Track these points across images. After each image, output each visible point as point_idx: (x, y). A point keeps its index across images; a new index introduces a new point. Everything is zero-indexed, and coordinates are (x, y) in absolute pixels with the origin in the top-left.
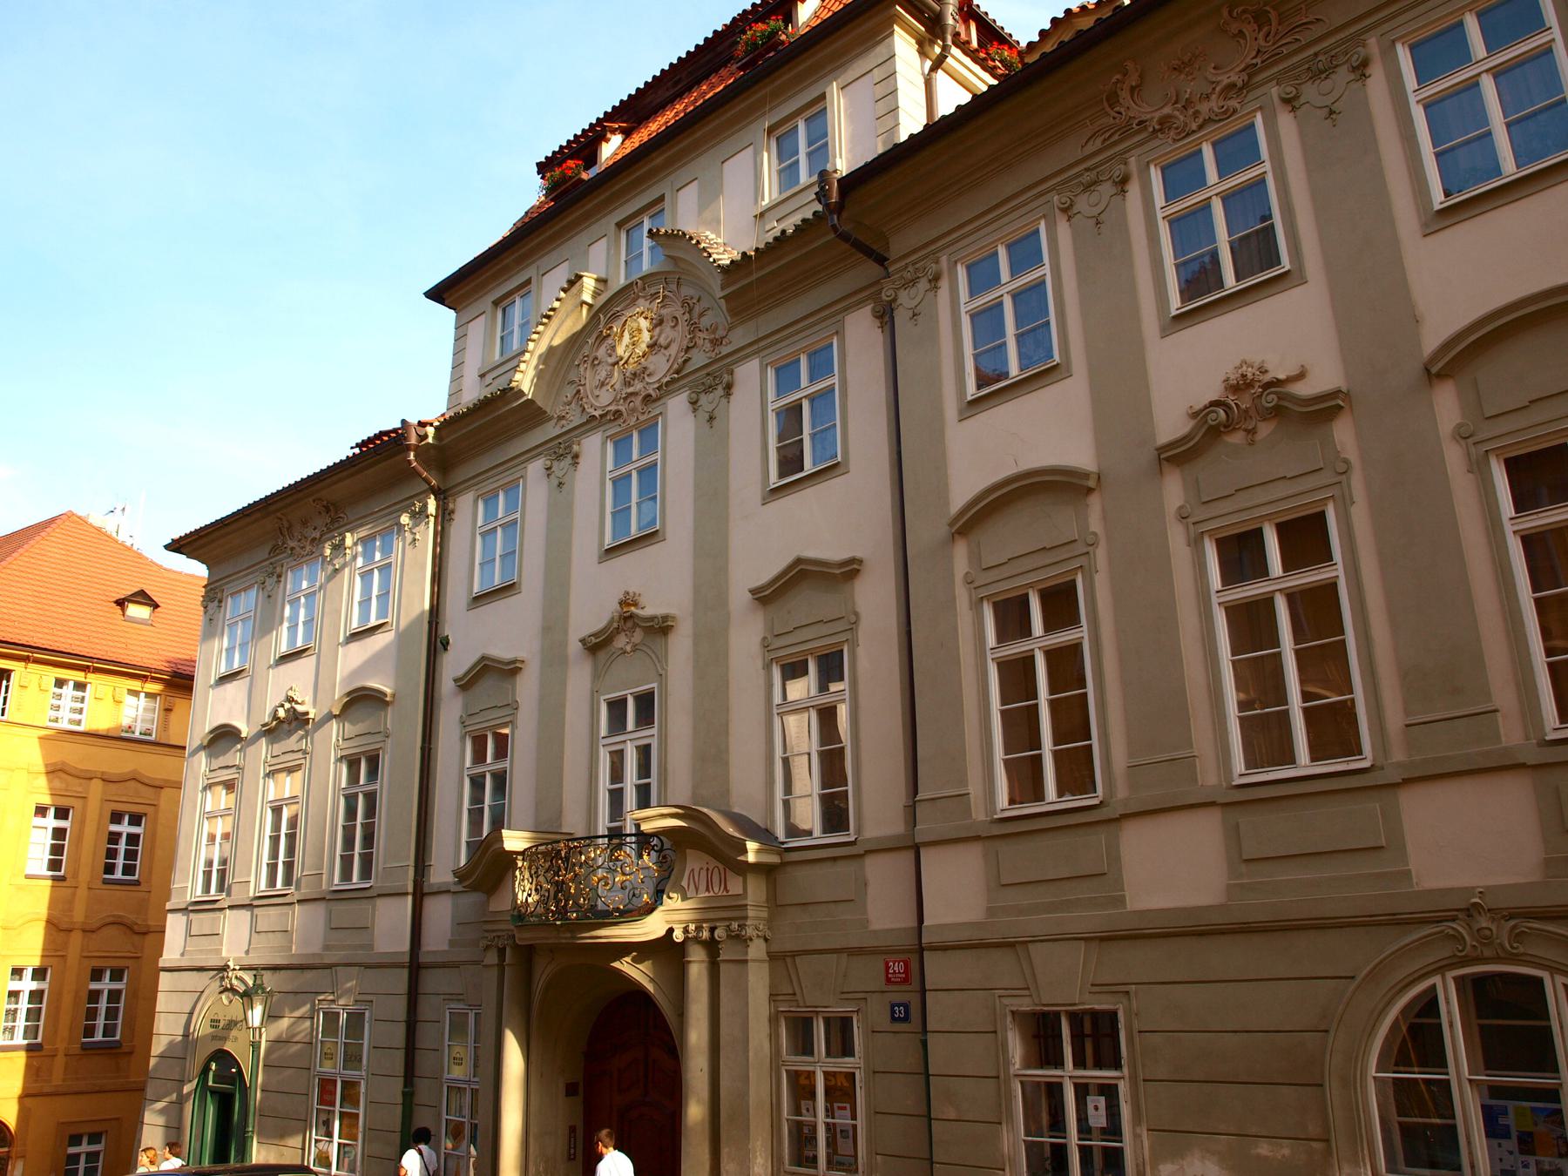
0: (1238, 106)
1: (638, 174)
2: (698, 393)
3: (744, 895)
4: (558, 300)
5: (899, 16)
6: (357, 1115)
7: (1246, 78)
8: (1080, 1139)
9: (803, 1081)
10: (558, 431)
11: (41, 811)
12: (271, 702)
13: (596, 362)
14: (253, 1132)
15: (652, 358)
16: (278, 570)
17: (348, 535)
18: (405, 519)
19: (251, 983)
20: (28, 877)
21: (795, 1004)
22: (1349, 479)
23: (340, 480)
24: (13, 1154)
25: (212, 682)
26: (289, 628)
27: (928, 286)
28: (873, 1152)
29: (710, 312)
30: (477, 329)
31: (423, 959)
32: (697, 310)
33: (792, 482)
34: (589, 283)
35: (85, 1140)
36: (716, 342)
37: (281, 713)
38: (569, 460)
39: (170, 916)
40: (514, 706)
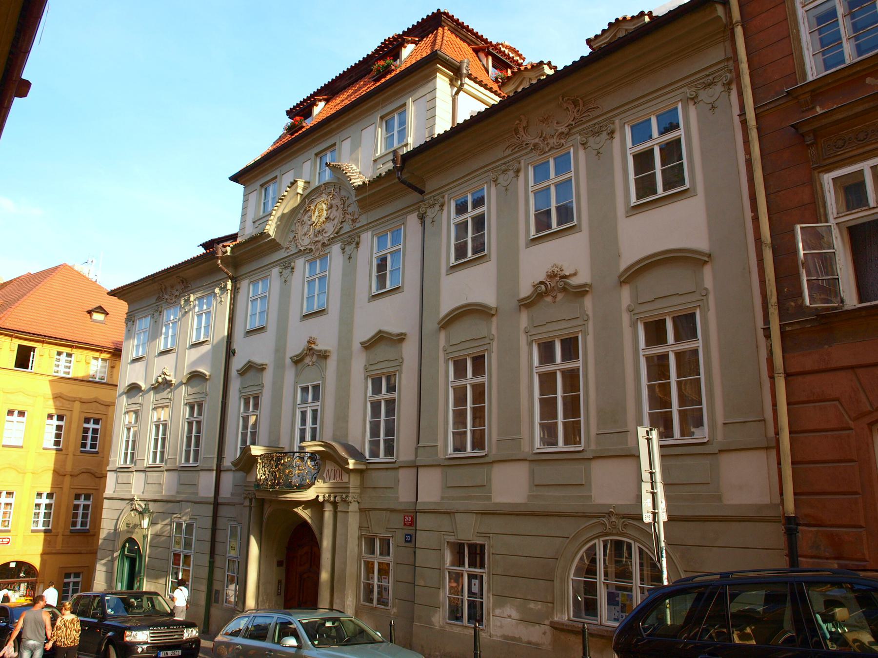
0: (564, 143)
1: (325, 131)
2: (345, 245)
3: (348, 483)
4: (286, 191)
5: (439, 69)
6: (189, 570)
7: (568, 130)
8: (468, 597)
9: (370, 566)
10: (286, 255)
11: (50, 417)
12: (155, 375)
14: (144, 576)
15: (327, 224)
16: (160, 309)
17: (192, 295)
18: (217, 290)
19: (144, 507)
20: (44, 449)
22: (588, 324)
23: (188, 269)
24: (38, 581)
25: (129, 361)
26: (164, 338)
27: (439, 209)
28: (395, 598)
29: (352, 205)
30: (253, 197)
31: (220, 501)
32: (346, 204)
33: (682, 191)
34: (301, 184)
35: (72, 576)
36: (354, 221)
37: (160, 380)
38: (289, 270)
39: (108, 473)
40: (262, 386)
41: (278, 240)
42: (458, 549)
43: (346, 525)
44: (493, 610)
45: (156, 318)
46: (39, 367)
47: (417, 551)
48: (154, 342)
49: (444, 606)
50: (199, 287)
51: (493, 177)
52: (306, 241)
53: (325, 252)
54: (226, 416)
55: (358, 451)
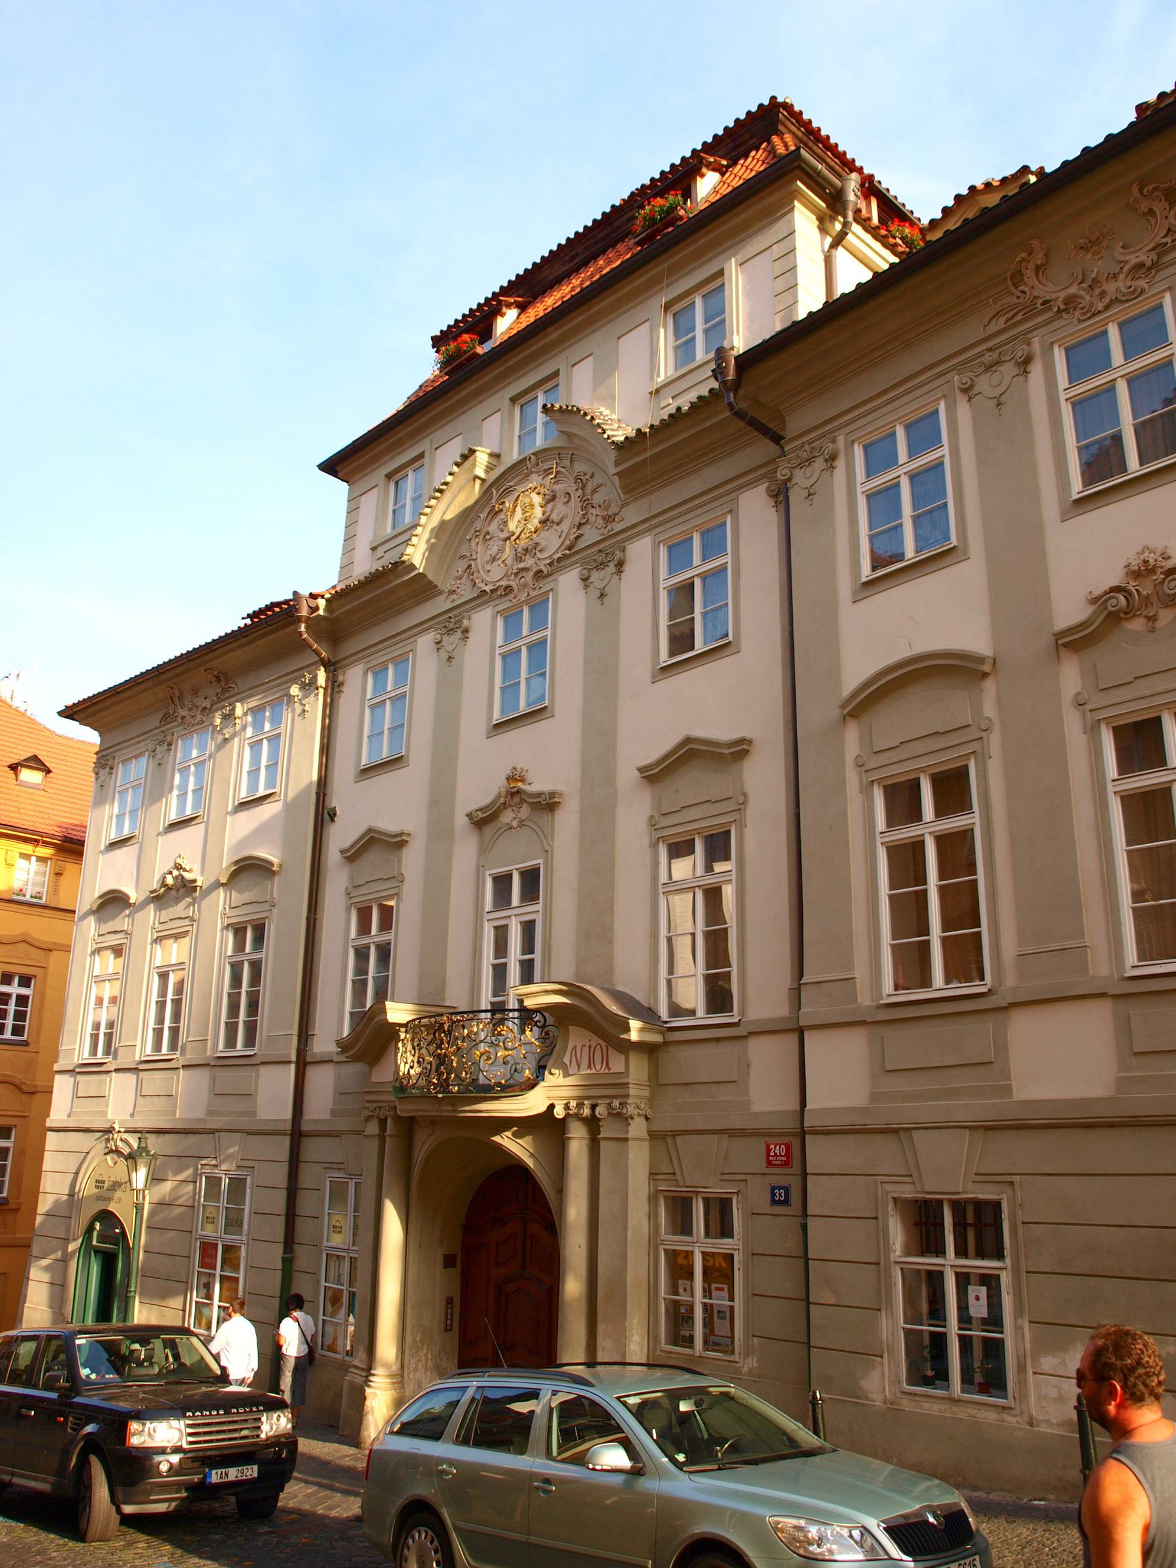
0: (1146, 286)
2: (589, 570)
3: (626, 1073)
4: (451, 474)
6: (237, 1279)
8: (960, 1329)
10: (448, 605)
12: (159, 869)
13: (488, 537)
14: (135, 1292)
15: (544, 534)
16: (169, 738)
17: (238, 705)
18: (295, 690)
21: (674, 1183)
23: (232, 650)
25: (102, 848)
26: (178, 796)
27: (824, 466)
28: (749, 1334)
29: (602, 489)
30: (369, 502)
32: (590, 487)
34: (482, 458)
36: (609, 519)
37: (170, 880)
39: (57, 1077)
41: (431, 577)
43: (622, 1171)
44: (1035, 1359)
45: (159, 756)
47: (811, 1222)
48: (155, 807)
49: (891, 1349)
50: (255, 687)
51: (964, 381)
53: (542, 591)
54: (316, 950)
55: (643, 1006)
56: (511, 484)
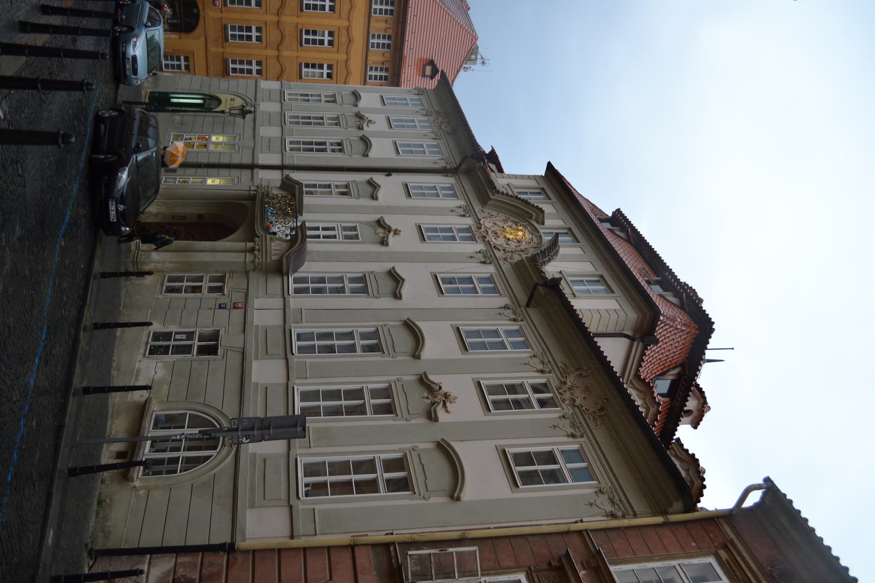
0: (566, 403)
10: (477, 210)
27: (569, 433)
31: (256, 170)
32: (521, 253)
33: (484, 395)
35: (186, 63)
36: (505, 259)
42: (215, 336)
45: (421, 112)
46: (376, 20)
51: (605, 489)
52: (487, 225)
56: (529, 228)
